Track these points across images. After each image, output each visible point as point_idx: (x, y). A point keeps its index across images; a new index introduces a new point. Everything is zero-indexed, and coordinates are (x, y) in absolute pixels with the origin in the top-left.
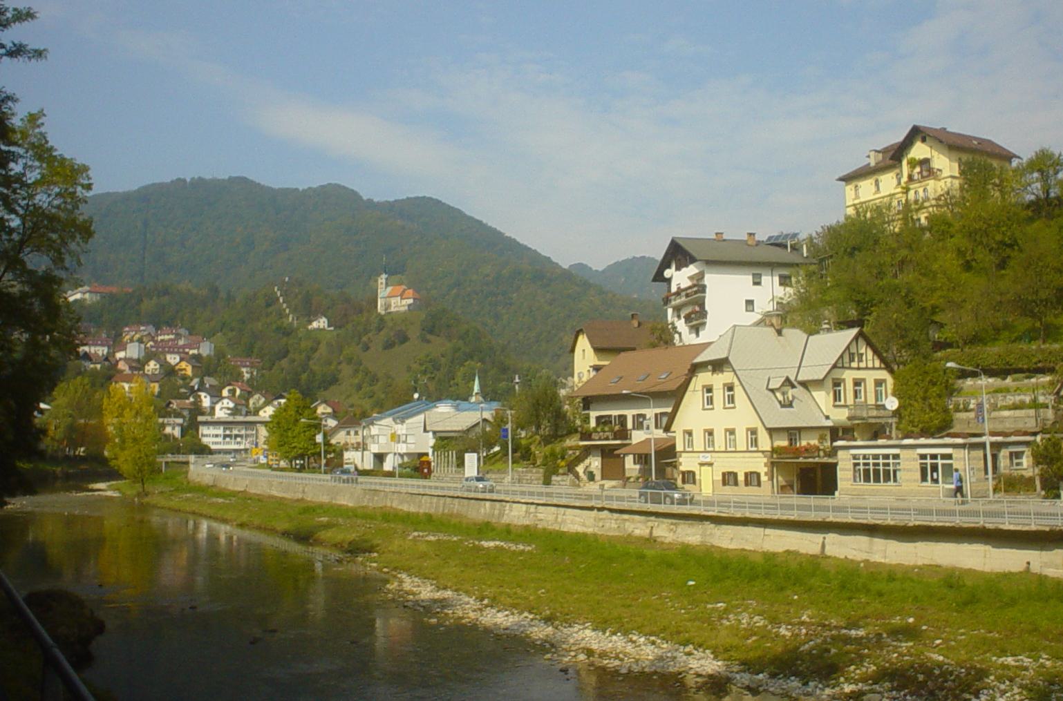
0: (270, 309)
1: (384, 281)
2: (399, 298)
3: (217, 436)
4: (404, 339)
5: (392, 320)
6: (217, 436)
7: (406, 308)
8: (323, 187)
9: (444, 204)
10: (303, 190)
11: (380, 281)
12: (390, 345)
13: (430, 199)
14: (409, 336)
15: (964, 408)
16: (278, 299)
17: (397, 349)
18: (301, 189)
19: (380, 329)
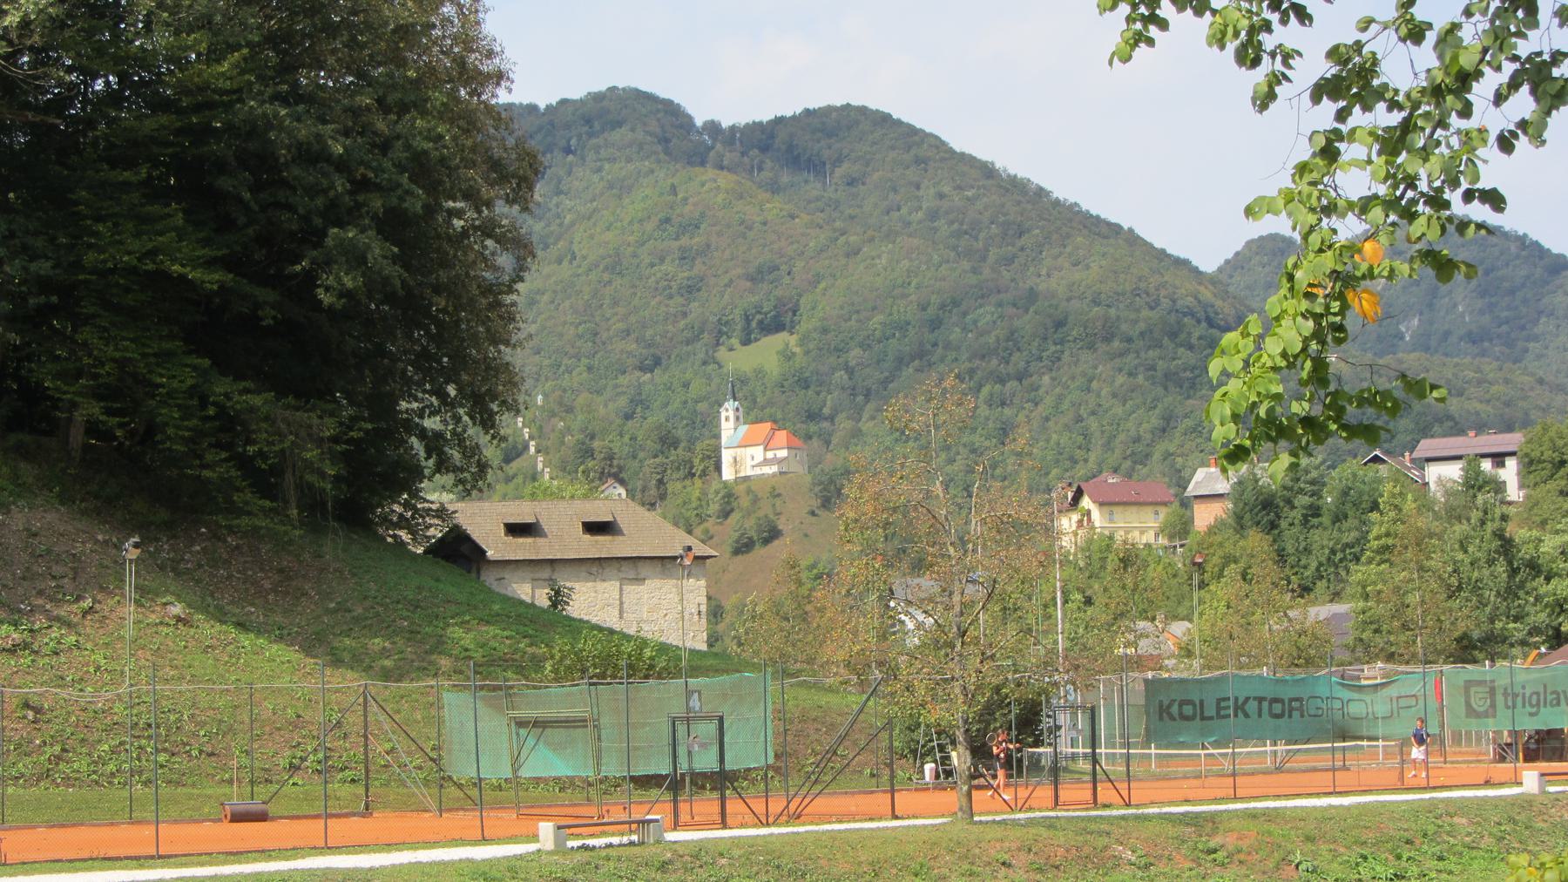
0: (515, 465)
1: (731, 414)
2: (761, 447)
3: (1455, 753)
4: (772, 534)
5: (749, 491)
6: (1455, 753)
7: (215, 287)
8: (597, 98)
9: (899, 123)
10: (549, 107)
11: (723, 414)
12: (746, 545)
13: (863, 110)
14: (780, 527)
15: (1424, 148)
16: (526, 447)
17: (759, 552)
18: (542, 106)
19: (726, 514)
